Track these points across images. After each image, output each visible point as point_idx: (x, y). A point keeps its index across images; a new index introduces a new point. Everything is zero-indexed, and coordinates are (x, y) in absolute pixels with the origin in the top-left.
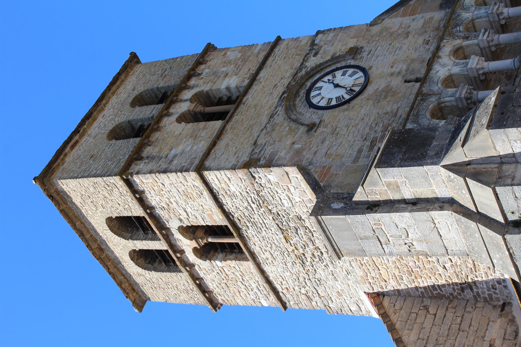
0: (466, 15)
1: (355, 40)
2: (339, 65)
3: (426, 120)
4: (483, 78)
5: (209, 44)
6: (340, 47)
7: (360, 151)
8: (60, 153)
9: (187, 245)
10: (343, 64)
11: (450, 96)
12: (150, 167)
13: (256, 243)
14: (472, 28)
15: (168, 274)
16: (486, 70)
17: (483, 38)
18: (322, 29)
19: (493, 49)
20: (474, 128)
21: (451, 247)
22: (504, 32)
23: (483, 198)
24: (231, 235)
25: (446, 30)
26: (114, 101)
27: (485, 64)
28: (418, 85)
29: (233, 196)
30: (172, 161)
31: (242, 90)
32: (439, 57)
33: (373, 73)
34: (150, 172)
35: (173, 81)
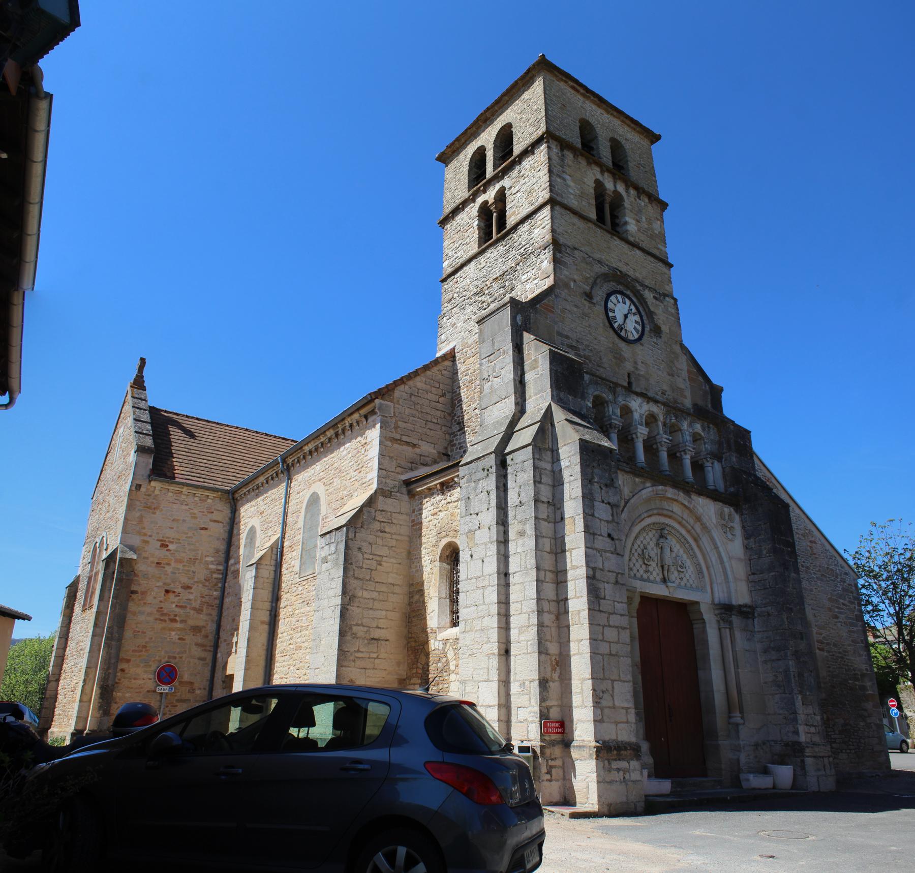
0: (685, 425)
1: (668, 331)
2: (645, 318)
3: (592, 392)
4: (629, 438)
5: (667, 205)
6: (661, 318)
7: (567, 337)
8: (567, 77)
9: (490, 195)
10: (646, 322)
11: (613, 412)
12: (554, 157)
13: (492, 254)
14: (673, 430)
15: (466, 181)
16: (636, 440)
17: (664, 438)
18: (678, 303)
19: (655, 446)
20: (581, 428)
21: (487, 412)
22: (669, 455)
23: (525, 436)
24: (499, 232)
25: (673, 408)
26: (616, 122)
27: (641, 440)
28: (626, 384)
29: (530, 232)
30: (560, 177)
31: (624, 235)
32: (648, 402)
33: (638, 348)
34: (549, 159)
35: (634, 173)
